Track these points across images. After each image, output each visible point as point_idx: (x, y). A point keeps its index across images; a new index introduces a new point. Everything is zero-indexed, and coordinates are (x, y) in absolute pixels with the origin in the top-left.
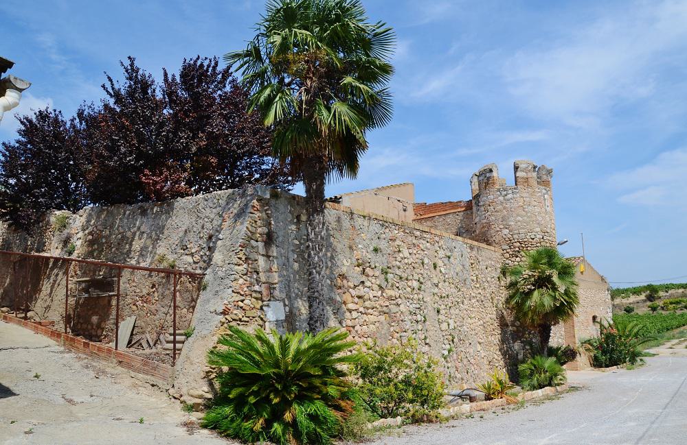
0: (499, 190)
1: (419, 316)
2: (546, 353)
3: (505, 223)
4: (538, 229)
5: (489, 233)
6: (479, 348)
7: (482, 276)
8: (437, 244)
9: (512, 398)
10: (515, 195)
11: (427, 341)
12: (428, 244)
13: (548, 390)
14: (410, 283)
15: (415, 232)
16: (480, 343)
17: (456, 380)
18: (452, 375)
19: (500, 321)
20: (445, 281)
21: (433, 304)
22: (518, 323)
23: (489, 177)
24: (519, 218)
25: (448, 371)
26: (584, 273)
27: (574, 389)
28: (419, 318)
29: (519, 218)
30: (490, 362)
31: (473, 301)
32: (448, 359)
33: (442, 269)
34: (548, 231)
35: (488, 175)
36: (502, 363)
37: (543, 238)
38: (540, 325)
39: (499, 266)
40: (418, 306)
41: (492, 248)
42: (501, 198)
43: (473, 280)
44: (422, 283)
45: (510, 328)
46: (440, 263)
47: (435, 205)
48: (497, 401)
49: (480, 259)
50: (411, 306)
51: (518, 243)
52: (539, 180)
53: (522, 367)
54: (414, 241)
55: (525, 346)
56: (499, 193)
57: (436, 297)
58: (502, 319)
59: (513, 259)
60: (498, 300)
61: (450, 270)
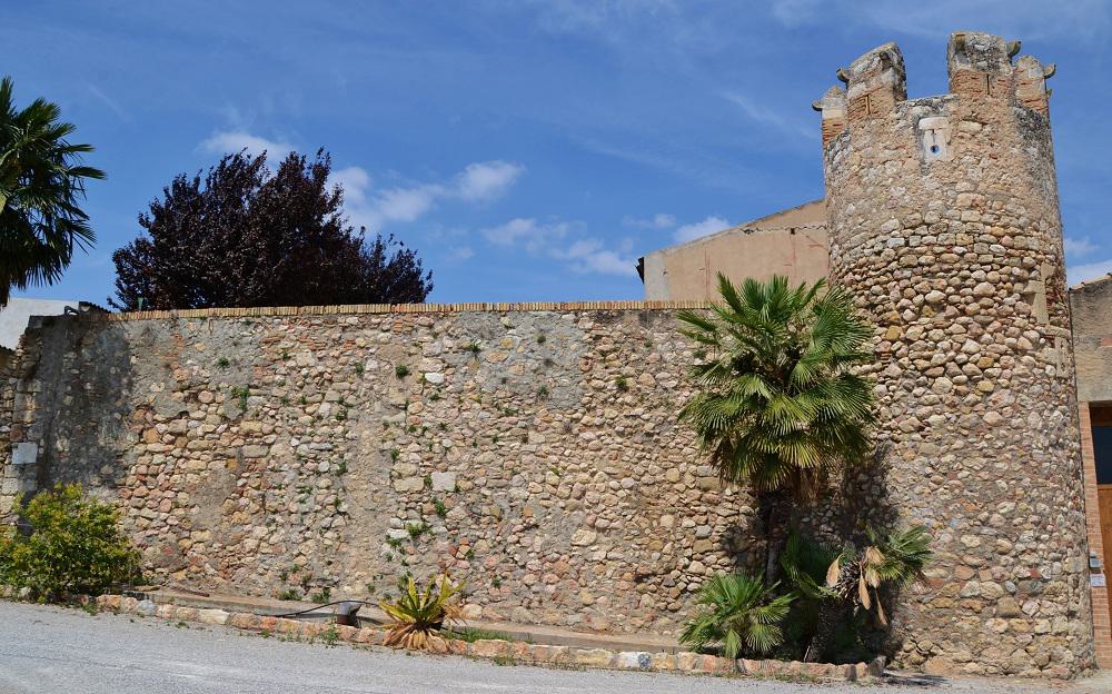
11: (344, 507)
37: (907, 244)
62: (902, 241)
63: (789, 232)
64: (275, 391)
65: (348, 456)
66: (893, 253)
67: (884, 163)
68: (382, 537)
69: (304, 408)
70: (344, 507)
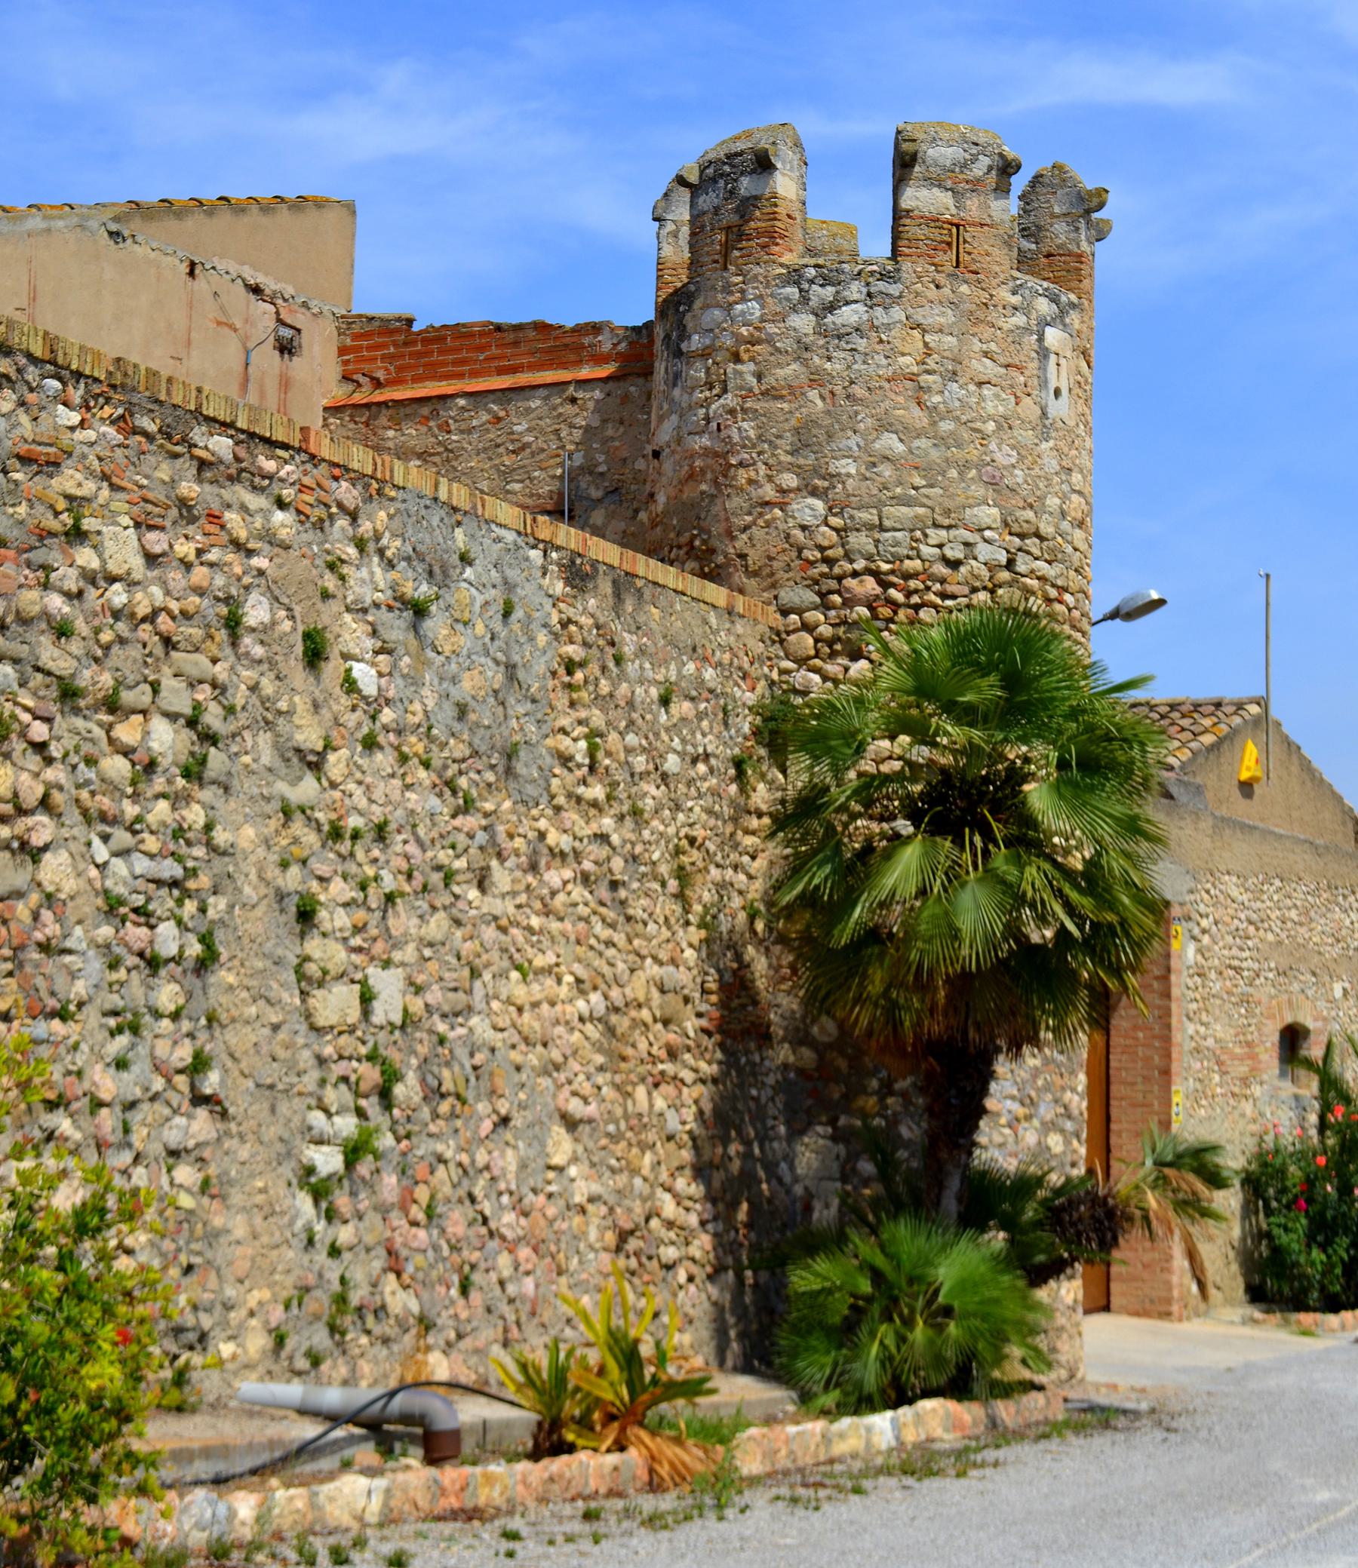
0: (794, 276)
1: (167, 930)
2: (950, 1204)
3: (808, 460)
4: (989, 514)
5: (716, 509)
6: (561, 1146)
7: (631, 739)
8: (342, 522)
9: (691, 1456)
10: (879, 311)
11: (212, 1081)
12: (279, 516)
13: (934, 1418)
14: (127, 732)
15: (198, 434)
16: (571, 1123)
17: (377, 1330)
18: (355, 1298)
19: (723, 1005)
20: (370, 744)
21: (273, 872)
22: (825, 1029)
23: (753, 200)
24: (890, 442)
25: (333, 1272)
26: (1257, 789)
27: (1098, 1418)
28: (167, 939)
29: (890, 442)
30: (624, 1236)
31: (554, 877)
32: (342, 1201)
33: (359, 670)
34: (1046, 529)
35: (746, 185)
36: (702, 1244)
37: (1010, 565)
38: (931, 1047)
39: (750, 698)
40: (170, 869)
41: (717, 593)
42: (803, 322)
43: (565, 760)
44: (210, 738)
45: (783, 1053)
46: (351, 634)
47: (460, 333)
48: (590, 1465)
49: (629, 643)
50: (119, 866)
51: (870, 582)
52: (1028, 245)
53: (804, 1279)
54: (189, 488)
55: (852, 1157)
56: (792, 291)
57: (298, 827)
58: (735, 990)
59: (832, 668)
60: (722, 886)
61: (414, 681)
62: (1003, 557)
63: (184, 268)
64: (50, 654)
65: (217, 906)
66: (985, 573)
67: (980, 384)
68: (287, 1171)
69: (109, 728)
70: (212, 1081)
